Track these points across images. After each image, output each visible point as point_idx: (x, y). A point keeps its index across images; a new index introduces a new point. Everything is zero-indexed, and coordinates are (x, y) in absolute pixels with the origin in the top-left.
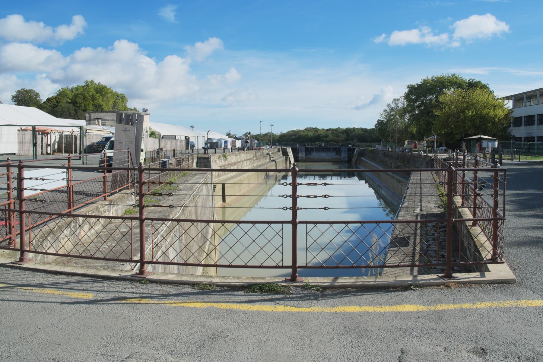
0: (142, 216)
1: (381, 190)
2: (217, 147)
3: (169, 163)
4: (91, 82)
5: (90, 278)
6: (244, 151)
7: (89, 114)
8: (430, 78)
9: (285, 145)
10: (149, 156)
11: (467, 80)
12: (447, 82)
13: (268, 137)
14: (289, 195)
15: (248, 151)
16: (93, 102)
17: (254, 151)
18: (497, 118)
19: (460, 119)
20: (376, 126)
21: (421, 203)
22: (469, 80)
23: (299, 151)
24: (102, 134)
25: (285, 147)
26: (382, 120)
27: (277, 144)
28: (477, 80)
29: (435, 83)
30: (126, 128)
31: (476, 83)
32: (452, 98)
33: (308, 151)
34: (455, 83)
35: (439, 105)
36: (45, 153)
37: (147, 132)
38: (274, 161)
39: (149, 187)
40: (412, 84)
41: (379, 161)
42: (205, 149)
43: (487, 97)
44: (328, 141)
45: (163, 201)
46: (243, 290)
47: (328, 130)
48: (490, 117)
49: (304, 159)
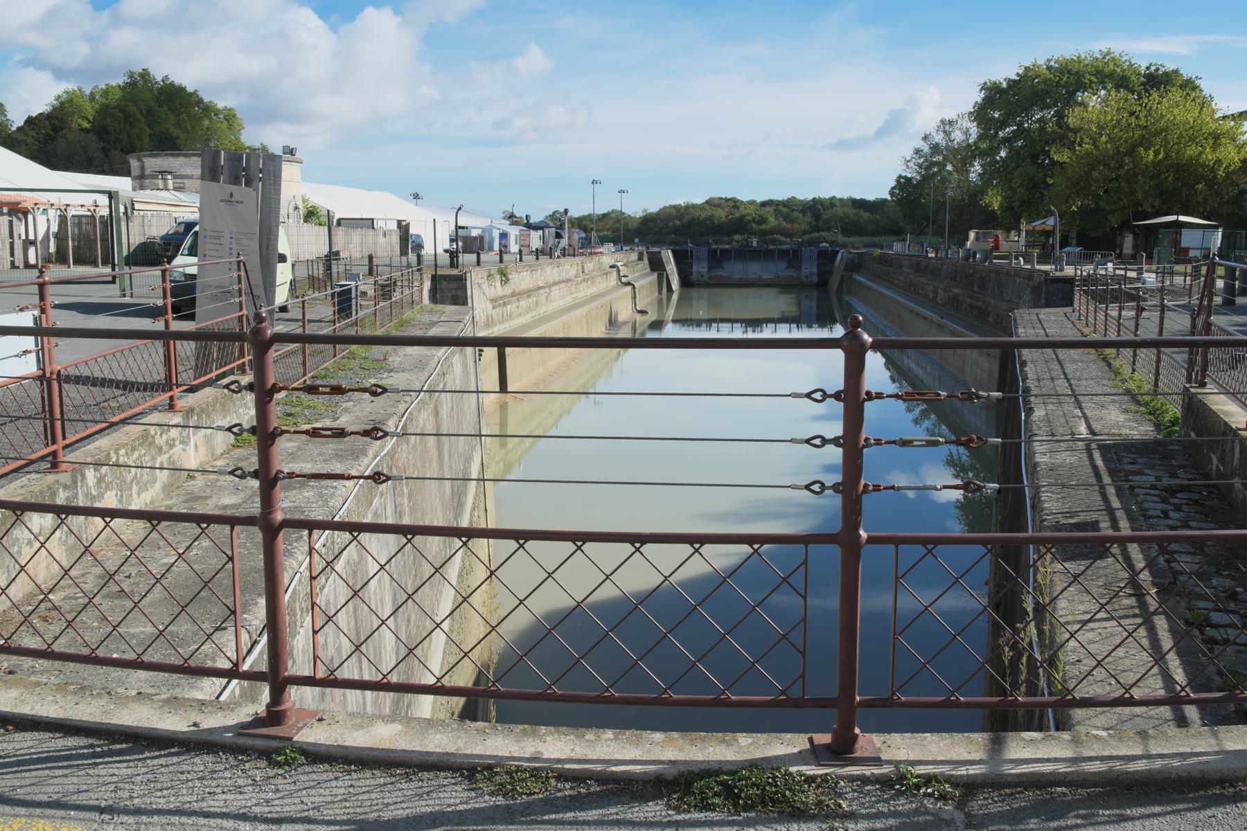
0: (270, 513)
1: (906, 361)
2: (482, 248)
3: (359, 294)
4: (141, 75)
5: (82, 741)
6: (551, 258)
7: (139, 160)
8: (1042, 63)
9: (657, 242)
10: (303, 273)
11: (1143, 67)
12: (1090, 74)
13: (610, 222)
14: (832, 437)
15: (562, 260)
16: (151, 128)
17: (578, 259)
18: (1222, 169)
19: (1123, 172)
20: (892, 193)
21: (1081, 408)
22: (1148, 68)
23: (692, 258)
24: (175, 215)
25: (658, 250)
26: (909, 176)
27: (636, 240)
28: (1170, 67)
29: (1055, 76)
30: (231, 195)
31: (1166, 74)
32: (1102, 117)
33: (716, 259)
34: (1111, 75)
35: (1065, 135)
36: (22, 266)
37: (296, 208)
38: (628, 284)
39: (304, 364)
40: (993, 79)
41: (901, 285)
42: (453, 255)
43: (1197, 111)
44: (764, 233)
45: (345, 404)
46: (661, 798)
47: (764, 204)
48: (1203, 166)
49: (705, 278)
